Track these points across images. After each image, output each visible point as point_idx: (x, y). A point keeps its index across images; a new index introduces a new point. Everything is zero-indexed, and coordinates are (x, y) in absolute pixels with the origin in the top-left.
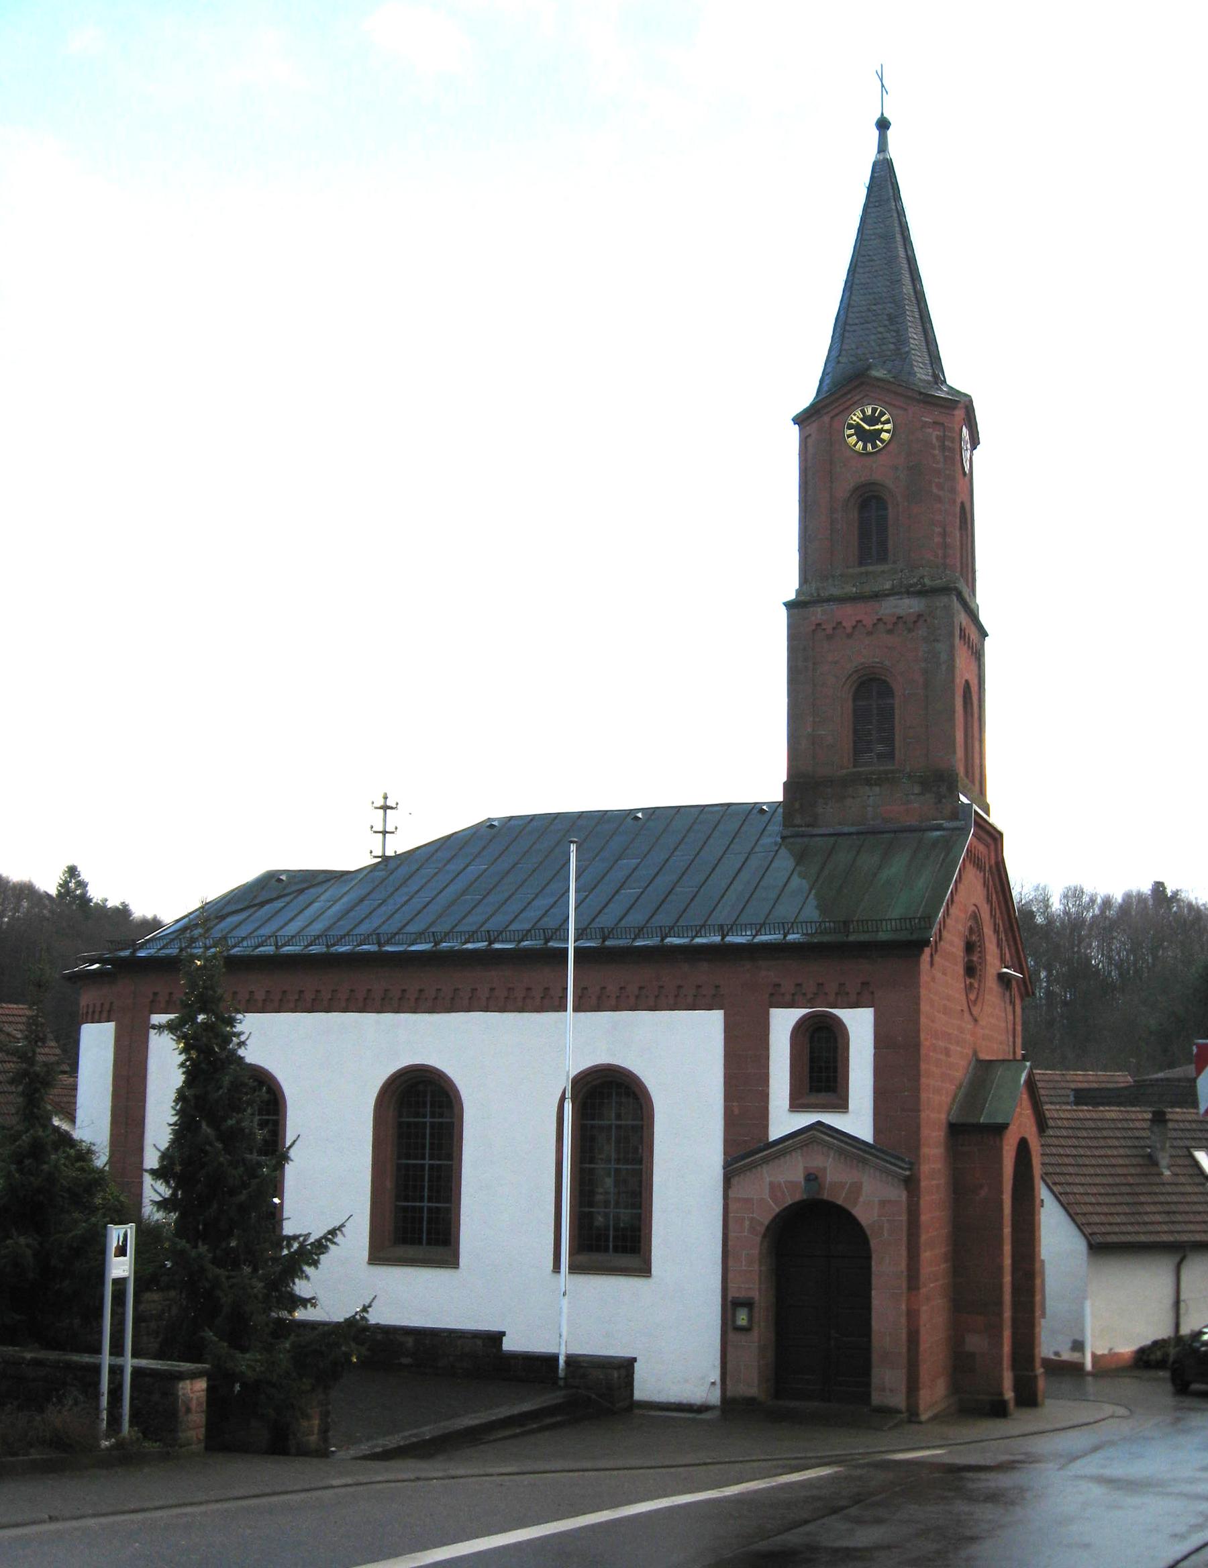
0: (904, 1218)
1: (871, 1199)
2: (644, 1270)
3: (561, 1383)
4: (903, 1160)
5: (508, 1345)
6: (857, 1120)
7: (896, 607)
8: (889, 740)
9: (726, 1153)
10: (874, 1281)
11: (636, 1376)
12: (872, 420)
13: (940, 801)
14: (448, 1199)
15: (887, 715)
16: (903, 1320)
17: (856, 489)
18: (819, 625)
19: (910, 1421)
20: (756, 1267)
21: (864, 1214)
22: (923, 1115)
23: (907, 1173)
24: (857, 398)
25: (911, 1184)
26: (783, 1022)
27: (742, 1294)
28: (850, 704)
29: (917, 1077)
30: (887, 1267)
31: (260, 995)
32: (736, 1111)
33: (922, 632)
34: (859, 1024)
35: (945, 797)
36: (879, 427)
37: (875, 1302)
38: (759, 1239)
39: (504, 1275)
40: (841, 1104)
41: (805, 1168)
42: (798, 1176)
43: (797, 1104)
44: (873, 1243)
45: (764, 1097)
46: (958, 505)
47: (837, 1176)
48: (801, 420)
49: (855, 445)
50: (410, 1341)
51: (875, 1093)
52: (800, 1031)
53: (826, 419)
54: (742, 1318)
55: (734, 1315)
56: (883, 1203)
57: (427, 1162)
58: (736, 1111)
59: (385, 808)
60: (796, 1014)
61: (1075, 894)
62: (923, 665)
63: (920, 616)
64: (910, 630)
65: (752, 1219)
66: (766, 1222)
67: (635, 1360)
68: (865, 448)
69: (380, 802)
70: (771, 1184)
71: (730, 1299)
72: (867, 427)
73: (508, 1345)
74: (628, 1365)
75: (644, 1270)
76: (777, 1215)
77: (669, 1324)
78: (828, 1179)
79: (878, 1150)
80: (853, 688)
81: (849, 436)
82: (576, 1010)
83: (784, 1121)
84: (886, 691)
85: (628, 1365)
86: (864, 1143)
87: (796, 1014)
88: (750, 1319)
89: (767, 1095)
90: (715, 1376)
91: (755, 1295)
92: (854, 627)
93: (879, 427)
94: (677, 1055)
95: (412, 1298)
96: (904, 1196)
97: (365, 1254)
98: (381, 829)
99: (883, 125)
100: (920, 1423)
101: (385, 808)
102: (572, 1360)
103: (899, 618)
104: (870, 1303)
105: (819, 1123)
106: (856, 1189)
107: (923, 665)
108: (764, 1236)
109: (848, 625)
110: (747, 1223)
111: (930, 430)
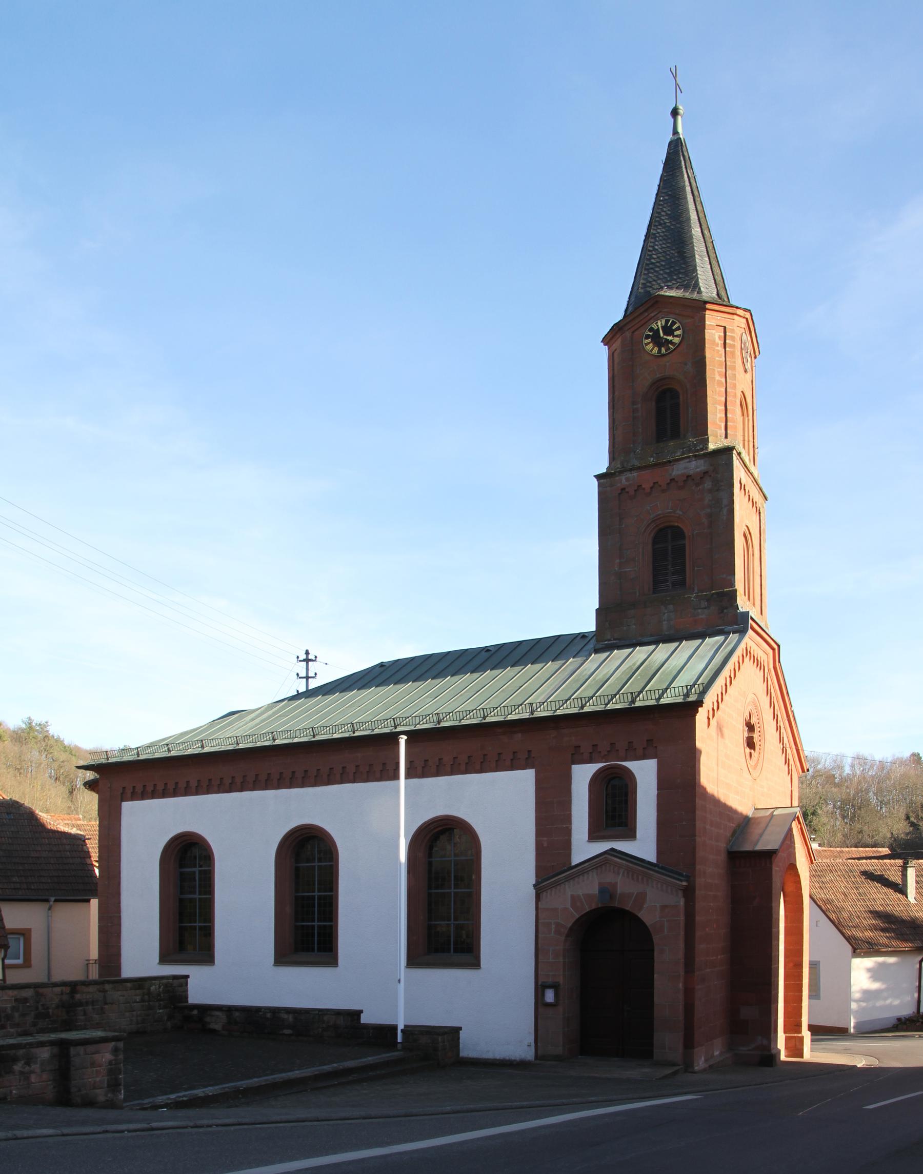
0: (682, 918)
1: (656, 905)
2: (475, 964)
3: (399, 1046)
4: (681, 875)
5: (364, 1019)
6: (644, 845)
7: (686, 468)
8: (682, 571)
9: (537, 875)
10: (657, 966)
11: (461, 1041)
12: (668, 330)
13: (722, 612)
14: (331, 920)
15: (680, 552)
16: (681, 996)
17: (654, 383)
18: (623, 489)
19: (686, 1071)
20: (561, 959)
21: (648, 917)
22: (698, 839)
23: (684, 883)
24: (652, 315)
25: (689, 893)
26: (582, 775)
27: (550, 981)
28: (649, 548)
29: (693, 811)
30: (667, 956)
31: (193, 784)
32: (545, 845)
33: (708, 484)
34: (645, 773)
35: (726, 608)
36: (670, 338)
37: (657, 983)
38: (563, 938)
39: (374, 971)
40: (630, 833)
41: (600, 884)
42: (595, 890)
43: (595, 835)
44: (656, 939)
45: (568, 832)
46: (739, 394)
47: (624, 886)
48: (607, 340)
49: (651, 351)
50: (290, 1018)
51: (658, 824)
52: (595, 781)
53: (628, 334)
54: (550, 996)
55: (543, 995)
56: (663, 907)
57: (316, 894)
58: (545, 845)
59: (307, 660)
60: (593, 768)
61: (860, 760)
62: (709, 510)
63: (705, 473)
64: (697, 485)
65: (557, 924)
66: (569, 925)
67: (460, 1028)
68: (660, 351)
69: (303, 657)
70: (573, 897)
71: (540, 983)
72: (662, 335)
73: (364, 1019)
74: (456, 1030)
75: (475, 964)
76: (578, 920)
77: (494, 1001)
78: (619, 892)
79: (662, 868)
80: (652, 535)
81: (647, 344)
82: (408, 776)
83: (583, 848)
84: (678, 534)
85: (456, 1030)
86: (650, 863)
87: (593, 768)
88: (556, 995)
89: (570, 830)
90: (531, 1039)
91: (561, 980)
92: (651, 488)
93: (670, 338)
94: (499, 806)
95: (305, 988)
96: (682, 902)
97: (158, 961)
98: (304, 675)
99: (675, 113)
100: (695, 1073)
101: (307, 660)
102: (409, 1031)
103: (688, 477)
104: (653, 984)
105: (612, 850)
106: (641, 898)
107: (709, 510)
108: (567, 936)
109: (647, 486)
110: (553, 926)
111: (713, 332)
